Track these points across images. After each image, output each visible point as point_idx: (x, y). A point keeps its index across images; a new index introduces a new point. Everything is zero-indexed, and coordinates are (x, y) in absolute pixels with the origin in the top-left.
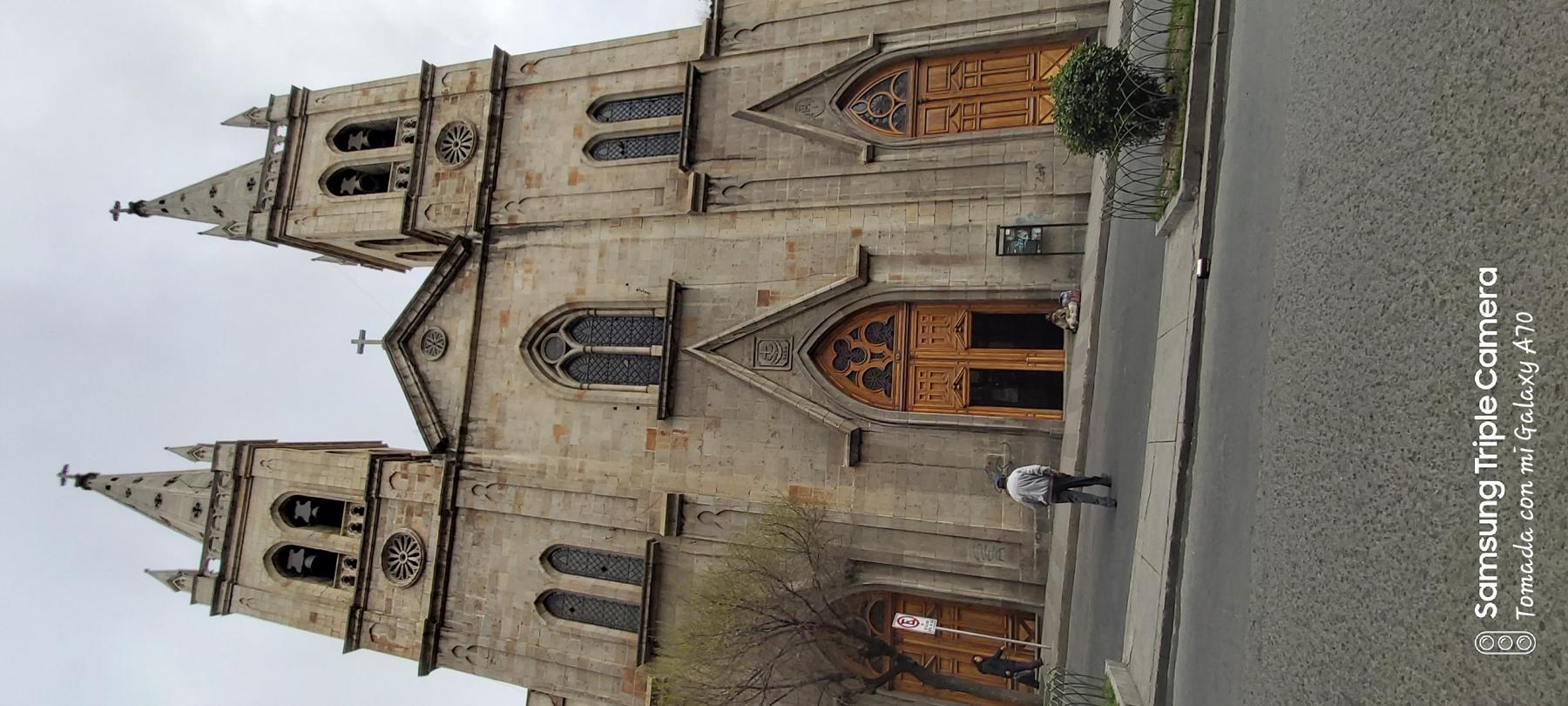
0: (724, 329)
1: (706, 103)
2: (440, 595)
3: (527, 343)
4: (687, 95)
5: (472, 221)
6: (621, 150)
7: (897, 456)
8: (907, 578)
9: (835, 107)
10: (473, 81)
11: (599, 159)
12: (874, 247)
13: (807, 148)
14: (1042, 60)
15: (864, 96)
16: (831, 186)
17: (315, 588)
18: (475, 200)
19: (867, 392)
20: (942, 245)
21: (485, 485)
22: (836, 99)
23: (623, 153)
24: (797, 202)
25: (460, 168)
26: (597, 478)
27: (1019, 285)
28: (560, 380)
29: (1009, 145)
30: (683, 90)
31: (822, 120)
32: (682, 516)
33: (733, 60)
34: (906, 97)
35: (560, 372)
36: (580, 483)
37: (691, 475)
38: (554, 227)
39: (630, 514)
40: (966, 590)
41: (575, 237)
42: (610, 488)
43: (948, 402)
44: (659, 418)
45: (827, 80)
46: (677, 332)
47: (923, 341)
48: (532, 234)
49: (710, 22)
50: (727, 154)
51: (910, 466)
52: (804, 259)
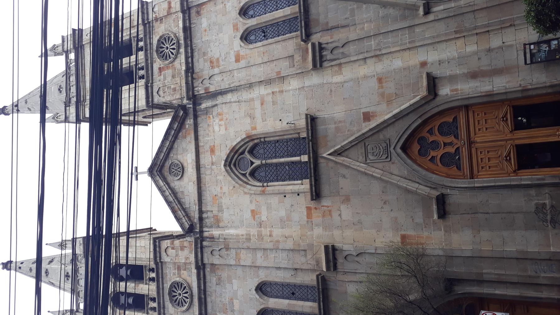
0: (344, 140)
3: (228, 163)
6: (263, 34)
10: (170, 7)
11: (251, 42)
12: (436, 72)
16: (401, 35)
19: (445, 169)
20: (485, 64)
21: (218, 249)
23: (264, 36)
25: (172, 62)
27: (545, 83)
28: (250, 183)
32: (335, 259)
35: (249, 178)
39: (303, 259)
40: (531, 293)
41: (245, 95)
43: (502, 169)
44: (312, 199)
47: (479, 130)
50: (330, 25)
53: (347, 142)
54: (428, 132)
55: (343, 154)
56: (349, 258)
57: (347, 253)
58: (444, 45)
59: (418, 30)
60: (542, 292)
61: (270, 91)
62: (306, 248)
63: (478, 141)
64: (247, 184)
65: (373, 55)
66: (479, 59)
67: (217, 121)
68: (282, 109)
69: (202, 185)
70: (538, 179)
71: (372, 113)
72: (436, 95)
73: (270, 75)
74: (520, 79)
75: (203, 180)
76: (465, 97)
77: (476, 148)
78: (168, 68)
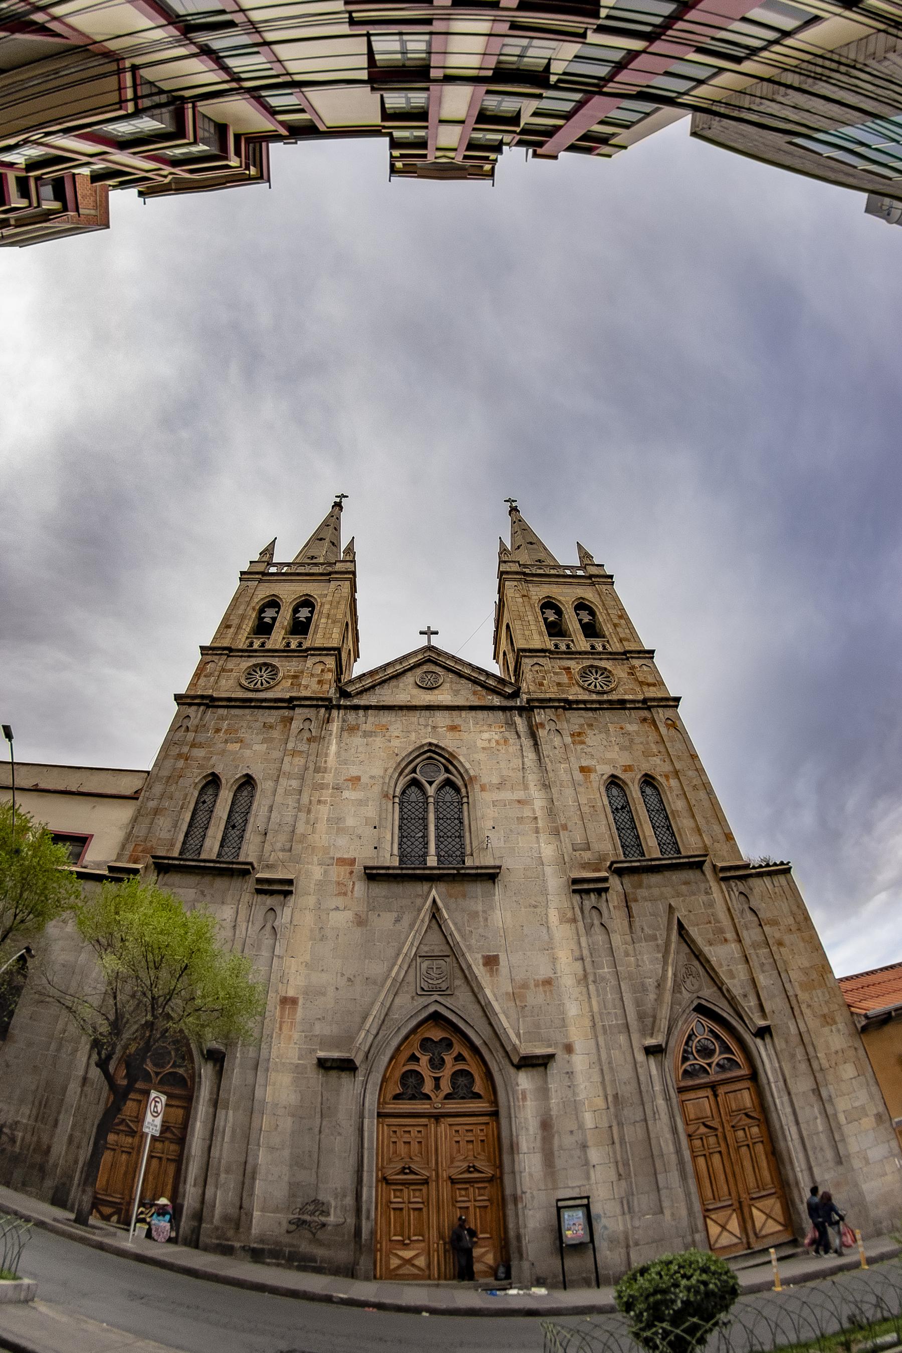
0: (455, 924)
1: (676, 877)
2: (231, 703)
3: (433, 748)
4: (680, 858)
5: (534, 696)
6: (619, 807)
7: (329, 1108)
8: (207, 1112)
9: (695, 1003)
10: (649, 685)
11: (608, 789)
12: (554, 1068)
13: (651, 982)
14: (771, 1201)
15: (711, 1031)
16: (616, 1013)
17: (248, 625)
18: (553, 696)
19: (398, 1074)
20: (564, 1141)
21: (311, 727)
22: (704, 1002)
23: (617, 809)
24: (594, 982)
25: (578, 684)
26: (312, 816)
27: (525, 1227)
28: (402, 778)
29: (680, 1192)
30: (684, 853)
31: (681, 993)
32: (272, 893)
33: (720, 895)
34: (717, 1073)
35: (408, 778)
36: (308, 803)
37: (311, 901)
38: (540, 760)
39: (279, 845)
40: (193, 1170)
41: (532, 778)
42: (301, 828)
43: (390, 1161)
44: (366, 868)
45: (720, 989)
46: (451, 878)
47: (457, 1131)
48: (532, 743)
49: (747, 866)
50: (633, 905)
51: (318, 1121)
52: (535, 998)
53: (453, 928)
54: (460, 1055)
55: (434, 921)
56: (271, 914)
57: (279, 912)
58: (597, 1078)
59: (622, 1039)
60: (195, 1185)
61: (539, 813)
62: (293, 852)
63: (439, 1129)
64: (400, 774)
65: (588, 971)
66: (572, 1132)
67: (496, 737)
68: (511, 831)
69: (405, 712)
70: (368, 1211)
71: (497, 970)
72: (518, 1068)
73: (561, 815)
74: (535, 1192)
75: (411, 713)
76: (512, 1111)
77: (426, 1125)
78: (571, 678)
